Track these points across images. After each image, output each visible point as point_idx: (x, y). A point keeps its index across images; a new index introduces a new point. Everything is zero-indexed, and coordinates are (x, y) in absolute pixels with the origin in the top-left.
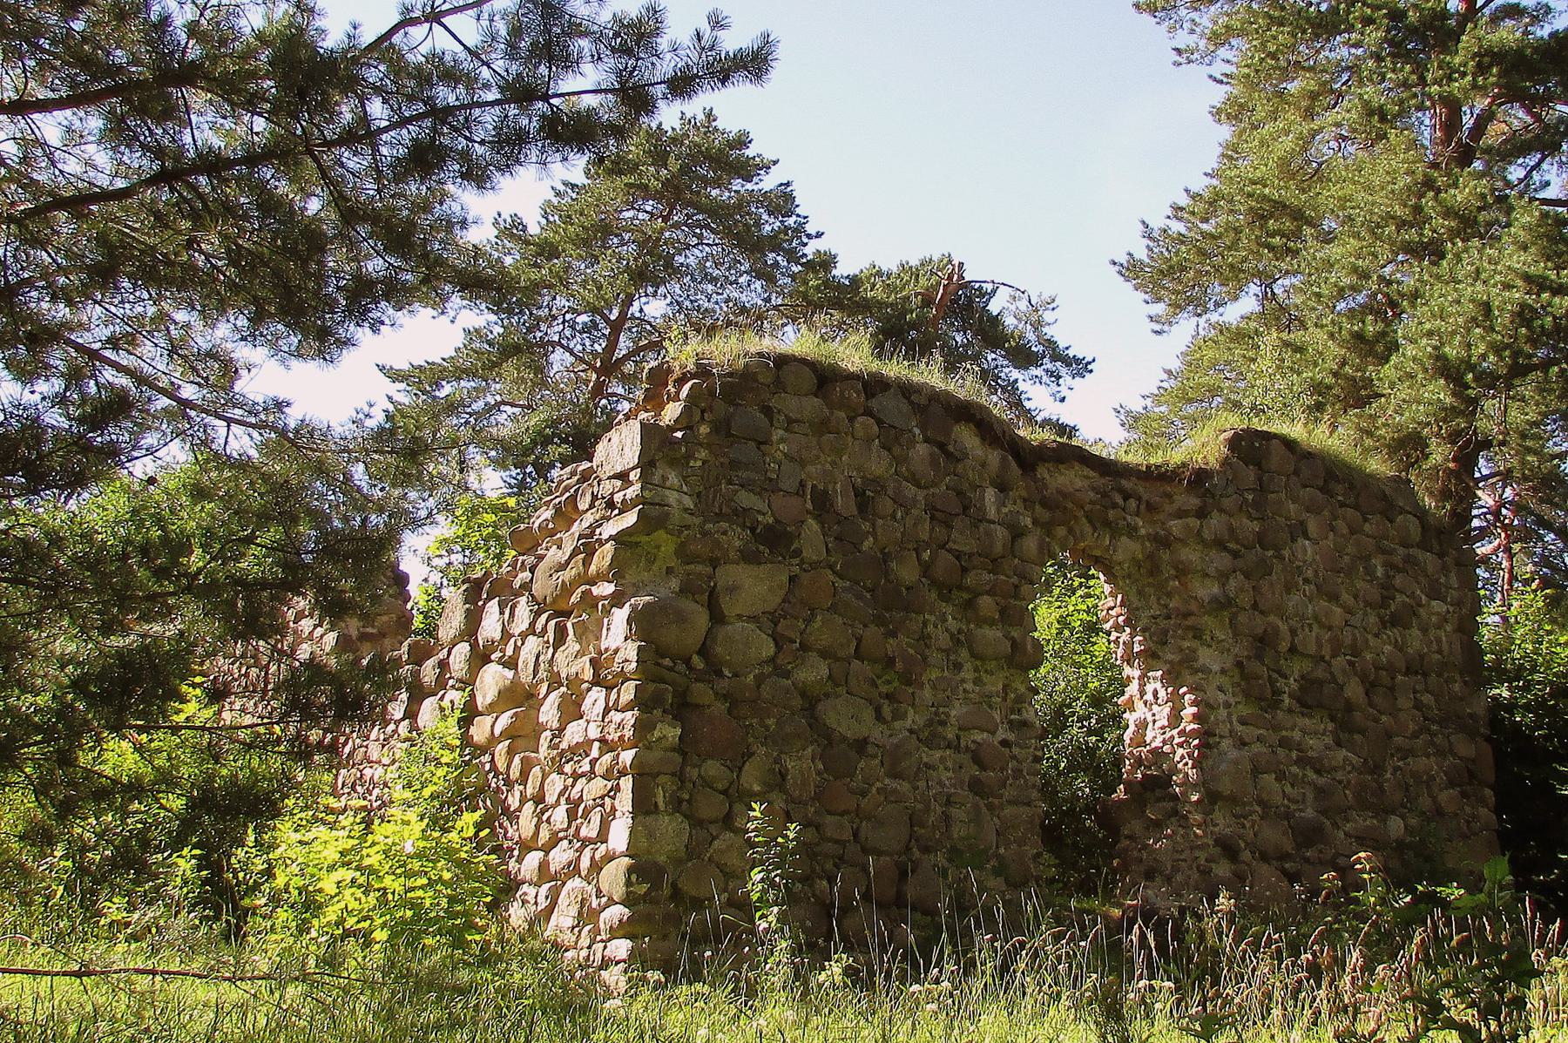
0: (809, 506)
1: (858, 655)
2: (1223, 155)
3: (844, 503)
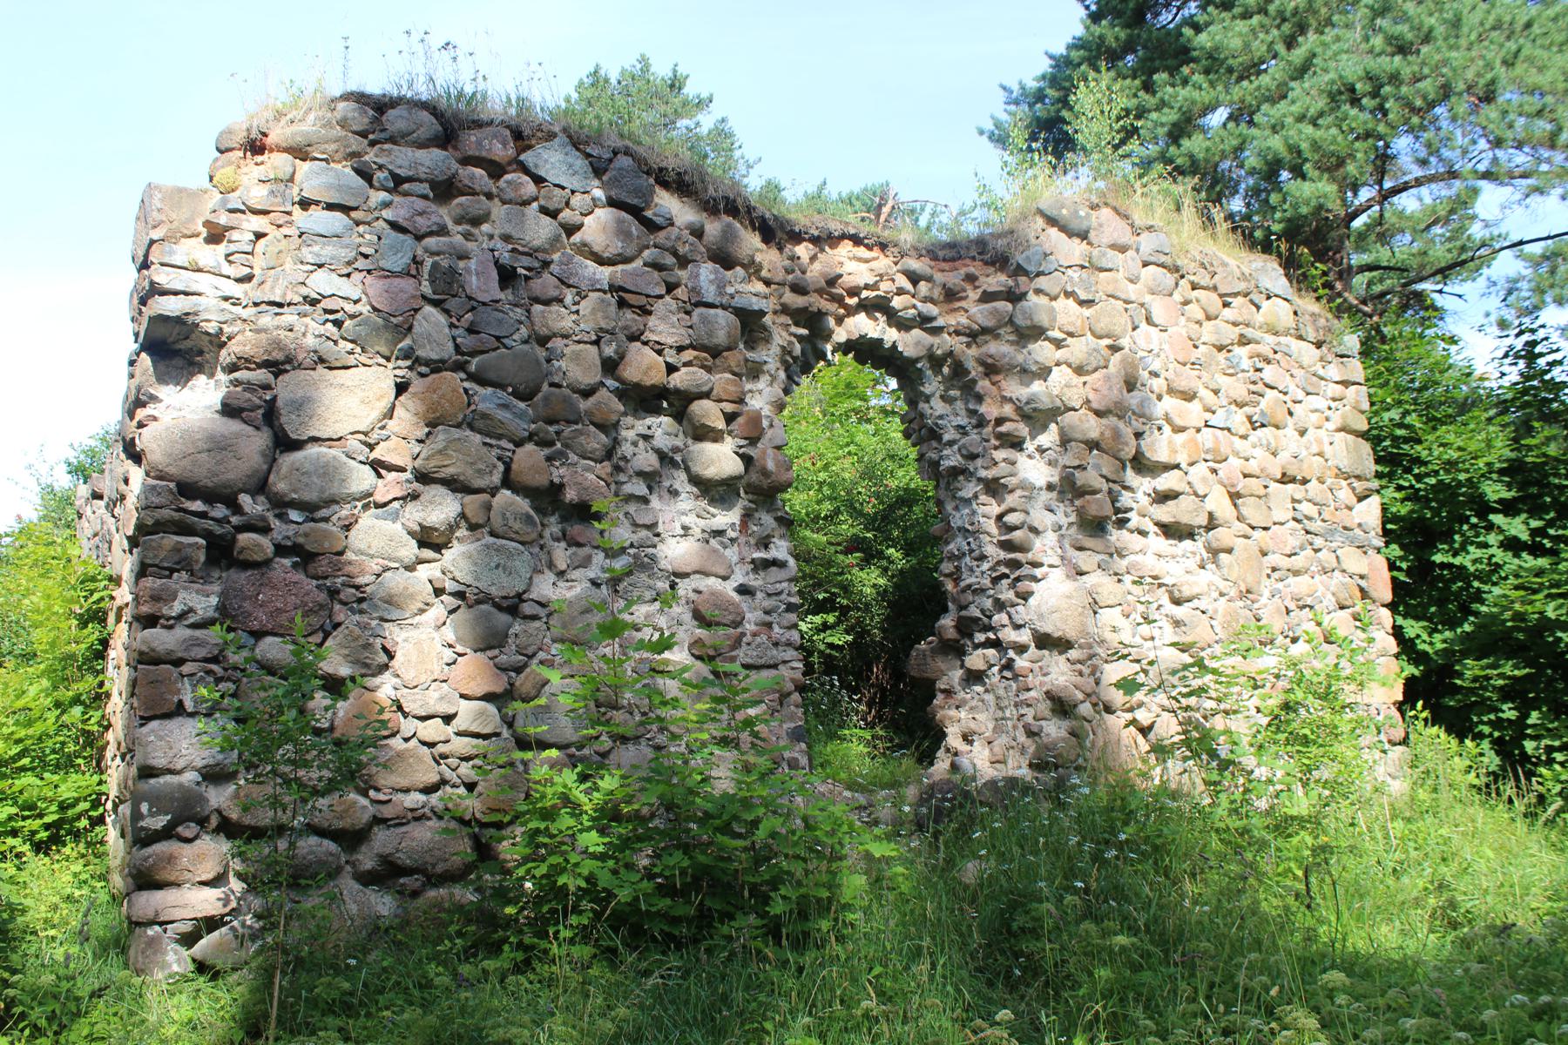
0: (426, 288)
1: (507, 482)
2: (1530, 815)
3: (480, 282)
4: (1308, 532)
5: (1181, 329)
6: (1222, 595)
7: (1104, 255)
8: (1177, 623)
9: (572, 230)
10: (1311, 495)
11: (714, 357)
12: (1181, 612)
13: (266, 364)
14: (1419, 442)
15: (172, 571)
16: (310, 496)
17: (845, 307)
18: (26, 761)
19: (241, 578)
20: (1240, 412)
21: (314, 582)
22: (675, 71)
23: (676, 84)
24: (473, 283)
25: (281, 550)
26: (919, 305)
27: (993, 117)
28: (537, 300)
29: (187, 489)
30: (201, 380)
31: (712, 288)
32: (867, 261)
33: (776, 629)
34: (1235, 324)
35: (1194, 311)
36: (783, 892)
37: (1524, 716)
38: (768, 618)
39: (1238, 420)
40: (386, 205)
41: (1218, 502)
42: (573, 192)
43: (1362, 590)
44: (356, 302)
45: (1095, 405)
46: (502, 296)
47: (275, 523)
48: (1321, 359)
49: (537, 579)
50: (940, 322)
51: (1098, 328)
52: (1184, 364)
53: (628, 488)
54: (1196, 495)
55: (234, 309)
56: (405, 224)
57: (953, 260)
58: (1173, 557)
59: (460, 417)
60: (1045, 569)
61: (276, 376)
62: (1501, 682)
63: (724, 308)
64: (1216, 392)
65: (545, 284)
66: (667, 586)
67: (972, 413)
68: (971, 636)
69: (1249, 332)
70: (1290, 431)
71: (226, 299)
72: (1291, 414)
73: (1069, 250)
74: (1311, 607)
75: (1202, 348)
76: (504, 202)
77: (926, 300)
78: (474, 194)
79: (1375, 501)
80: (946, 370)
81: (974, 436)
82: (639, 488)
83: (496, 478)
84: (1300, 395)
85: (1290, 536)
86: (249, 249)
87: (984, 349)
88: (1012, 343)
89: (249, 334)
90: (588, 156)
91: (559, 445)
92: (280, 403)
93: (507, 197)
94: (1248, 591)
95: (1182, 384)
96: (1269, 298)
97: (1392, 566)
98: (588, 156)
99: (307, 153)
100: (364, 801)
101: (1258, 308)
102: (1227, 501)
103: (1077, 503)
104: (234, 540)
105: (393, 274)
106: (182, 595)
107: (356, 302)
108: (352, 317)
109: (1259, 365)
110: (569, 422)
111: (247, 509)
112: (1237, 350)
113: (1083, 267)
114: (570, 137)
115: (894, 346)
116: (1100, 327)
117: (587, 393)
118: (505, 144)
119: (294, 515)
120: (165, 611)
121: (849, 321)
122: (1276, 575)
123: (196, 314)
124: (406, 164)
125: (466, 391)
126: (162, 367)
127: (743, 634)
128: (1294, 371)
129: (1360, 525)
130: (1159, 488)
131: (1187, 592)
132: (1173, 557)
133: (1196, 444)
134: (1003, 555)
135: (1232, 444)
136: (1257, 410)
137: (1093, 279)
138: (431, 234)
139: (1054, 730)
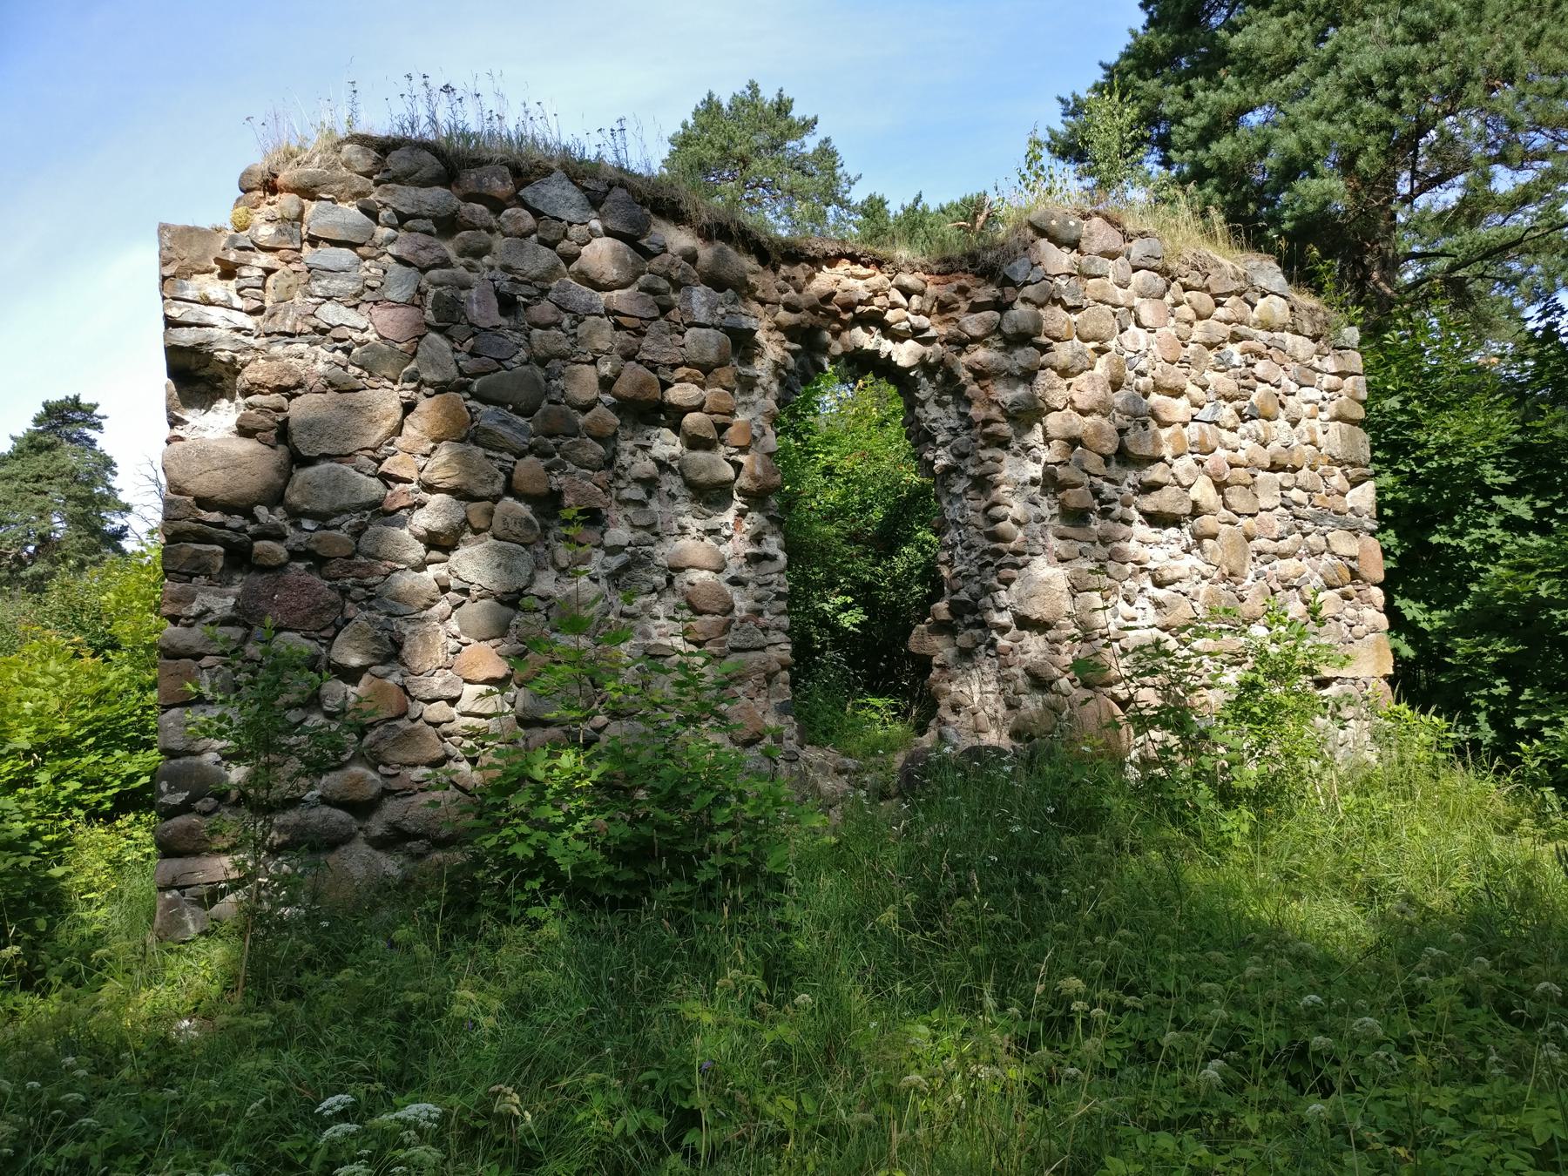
0: (429, 316)
3: (481, 309)
4: (1296, 517)
5: (1169, 330)
6: (1204, 577)
7: (1093, 262)
8: (1158, 605)
9: (570, 258)
10: (1301, 482)
11: (706, 373)
12: (1161, 594)
13: (279, 389)
14: (1421, 427)
15: (191, 576)
16: (322, 506)
17: (841, 322)
18: (91, 741)
19: (258, 580)
20: (1229, 406)
21: (327, 583)
22: (780, 96)
23: (783, 107)
24: (474, 310)
25: (295, 555)
26: (912, 317)
27: (1048, 129)
28: (536, 325)
29: (204, 502)
30: (224, 403)
31: (704, 310)
32: (863, 278)
33: (767, 615)
34: (1228, 322)
35: (1186, 312)
36: (711, 861)
37: (1517, 691)
38: (759, 606)
39: (1227, 412)
40: (392, 241)
41: (1203, 491)
42: (570, 224)
43: (1352, 570)
44: (363, 331)
45: (1078, 405)
46: (504, 321)
47: (290, 531)
48: (1318, 352)
49: (540, 576)
50: (932, 333)
51: (1085, 332)
52: (1173, 363)
53: (626, 494)
54: (1181, 486)
55: (246, 339)
56: (408, 258)
57: (946, 273)
58: (1157, 544)
59: (464, 433)
60: (1027, 557)
61: (289, 399)
62: (1492, 659)
63: (716, 328)
64: (1204, 388)
65: (544, 310)
66: (663, 580)
67: (963, 416)
68: (962, 617)
69: (1242, 329)
70: (1282, 422)
71: (238, 330)
72: (1282, 406)
73: (1058, 259)
74: (1298, 588)
75: (1192, 347)
76: (505, 235)
77: (917, 313)
78: (474, 228)
79: (1369, 487)
80: (939, 377)
81: (964, 437)
82: (637, 493)
83: (498, 487)
84: (1293, 387)
85: (1276, 522)
86: (259, 283)
87: (973, 356)
88: (1000, 349)
89: (261, 361)
90: (585, 189)
91: (558, 456)
92: (291, 424)
93: (507, 230)
94: (1231, 574)
95: (1169, 382)
96: (1264, 295)
97: (1386, 553)
98: (585, 189)
99: (314, 193)
100: (372, 775)
101: (1253, 306)
102: (1212, 490)
103: (1060, 496)
104: (251, 547)
105: (398, 304)
106: (200, 597)
107: (363, 331)
108: (360, 344)
109: (1251, 361)
110: (567, 435)
111: (262, 519)
112: (1229, 347)
113: (1070, 275)
114: (566, 172)
115: (889, 356)
116: (1086, 331)
117: (586, 408)
118: (504, 181)
119: (307, 524)
120: (184, 611)
121: (846, 335)
122: (1262, 558)
123: (209, 344)
124: (409, 202)
125: (469, 409)
126: (185, 392)
127: (732, 621)
128: (1287, 365)
129: (1352, 509)
130: (1145, 480)
131: (1168, 575)
132: (1157, 544)
133: (1182, 438)
134: (988, 545)
135: (1219, 435)
136: (1247, 403)
137: (1081, 286)
138: (435, 266)
139: (1032, 704)
